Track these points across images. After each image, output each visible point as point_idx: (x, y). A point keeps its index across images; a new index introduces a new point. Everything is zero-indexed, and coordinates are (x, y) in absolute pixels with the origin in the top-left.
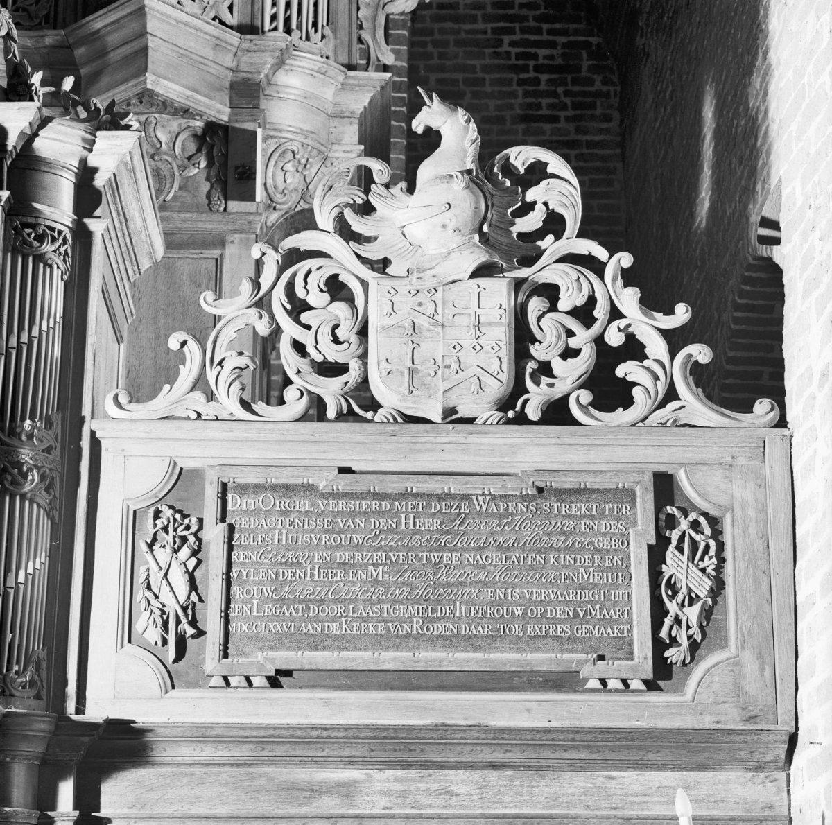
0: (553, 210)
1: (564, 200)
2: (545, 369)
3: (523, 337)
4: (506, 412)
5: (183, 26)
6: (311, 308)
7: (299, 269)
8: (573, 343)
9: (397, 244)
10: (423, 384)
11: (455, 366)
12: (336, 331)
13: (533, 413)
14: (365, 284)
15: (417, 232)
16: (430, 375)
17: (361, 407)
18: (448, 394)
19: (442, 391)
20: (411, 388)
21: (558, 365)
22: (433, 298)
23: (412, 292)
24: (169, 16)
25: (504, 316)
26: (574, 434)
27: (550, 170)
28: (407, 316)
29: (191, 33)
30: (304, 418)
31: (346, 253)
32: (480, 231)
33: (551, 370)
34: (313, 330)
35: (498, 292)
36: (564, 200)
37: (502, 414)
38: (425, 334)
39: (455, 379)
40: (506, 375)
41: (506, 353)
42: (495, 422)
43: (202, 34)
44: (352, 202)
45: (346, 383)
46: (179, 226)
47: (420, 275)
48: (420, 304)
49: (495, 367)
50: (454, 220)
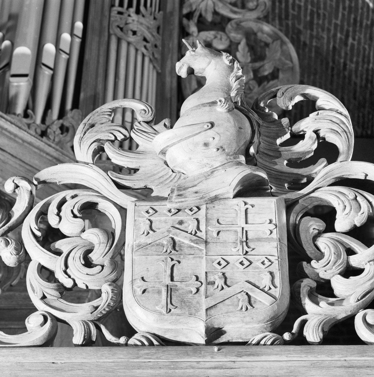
0: (324, 139)
1: (335, 127)
2: (324, 289)
3: (297, 256)
4: (281, 334)
5: (28, 145)
6: (64, 236)
7: (53, 199)
8: (354, 261)
9: (158, 173)
10: (182, 301)
11: (220, 282)
12: (90, 255)
13: (312, 334)
14: (123, 211)
15: (179, 156)
16: (191, 292)
17: (112, 333)
18: (212, 312)
19: (204, 308)
20: (170, 306)
21: (340, 285)
22: (196, 216)
23: (173, 210)
24: (16, 136)
25: (275, 231)
26: (362, 354)
27: (319, 103)
28: (166, 234)
29: (35, 152)
30: (48, 343)
31: (104, 182)
32: (247, 154)
33: (331, 290)
34: (64, 255)
35: (266, 212)
36: (335, 127)
37: (276, 336)
38: (186, 251)
39: (219, 295)
40: (281, 289)
41: (280, 269)
42: (269, 343)
43: (45, 155)
44: (113, 138)
45: (96, 308)
46: (21, 303)
47: (181, 193)
48: (181, 223)
49: (265, 281)
50: (217, 138)
